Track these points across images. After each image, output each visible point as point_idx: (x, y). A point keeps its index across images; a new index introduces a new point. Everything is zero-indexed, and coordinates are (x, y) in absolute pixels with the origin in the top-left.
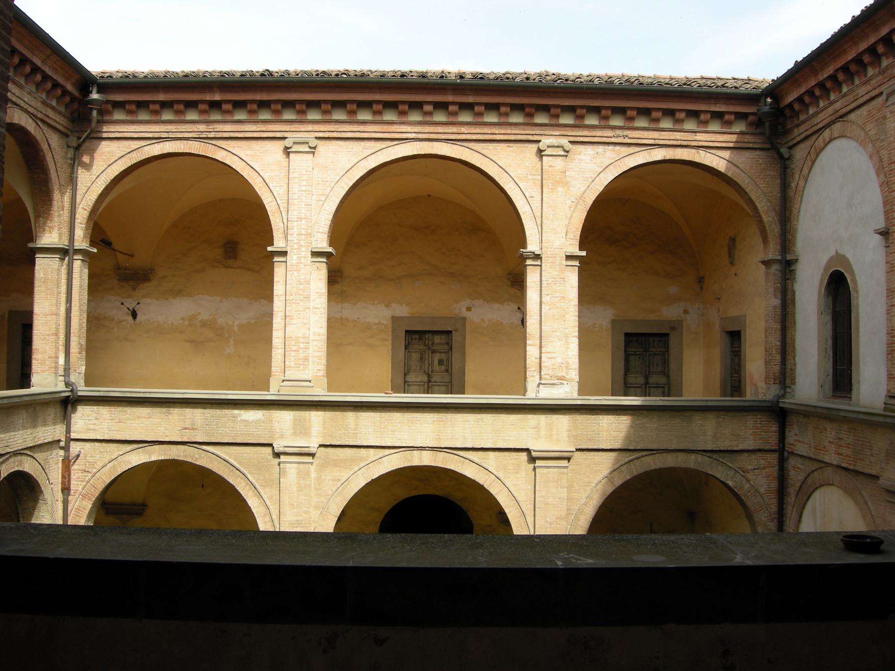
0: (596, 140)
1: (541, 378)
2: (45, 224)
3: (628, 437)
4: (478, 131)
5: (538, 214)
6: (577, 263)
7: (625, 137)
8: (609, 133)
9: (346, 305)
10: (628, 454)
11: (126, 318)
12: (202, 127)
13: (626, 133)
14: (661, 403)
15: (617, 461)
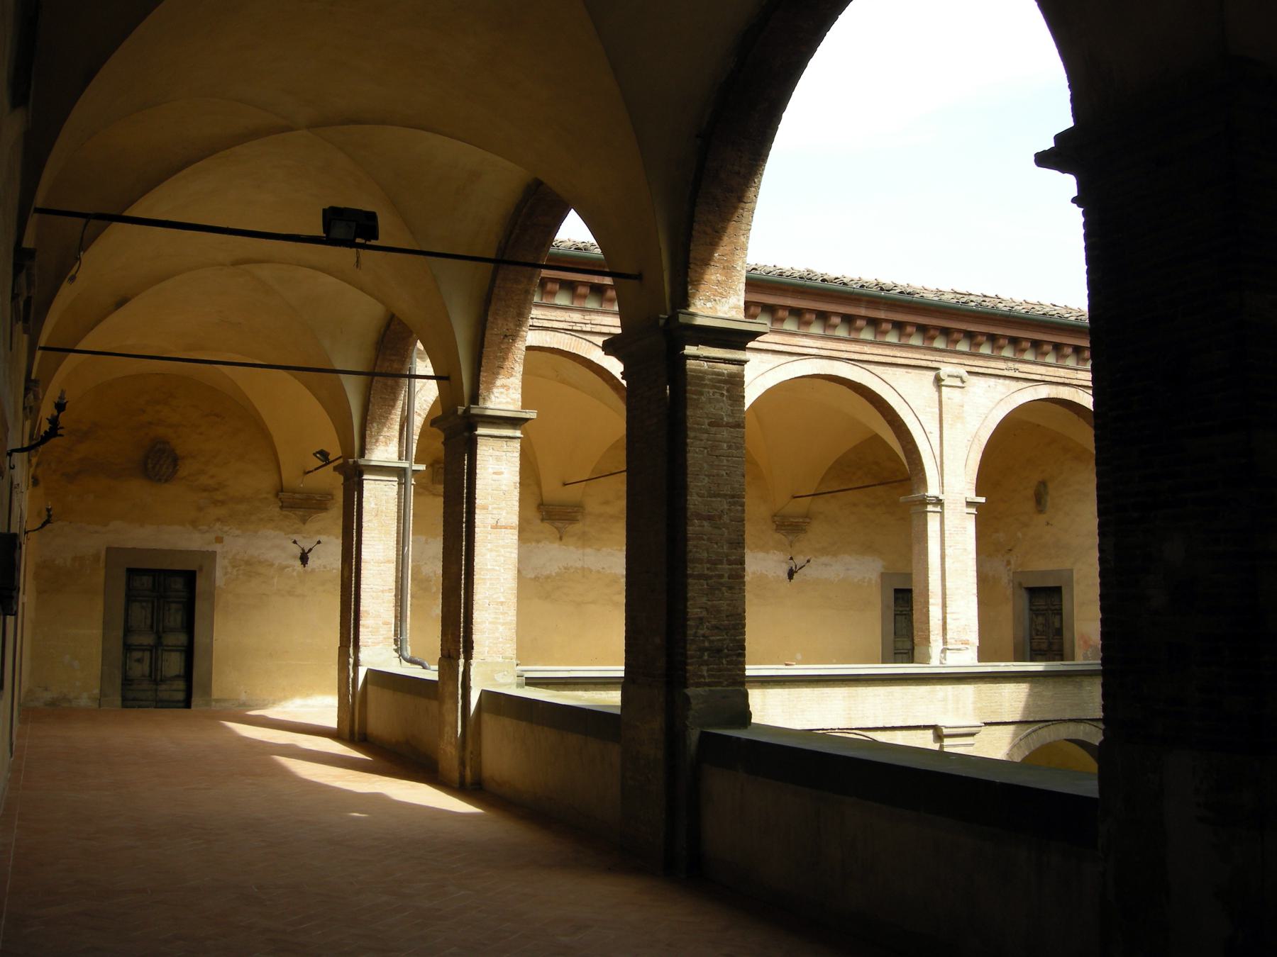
0: (989, 371)
1: (945, 642)
2: (379, 432)
3: (1027, 708)
4: (904, 355)
5: (937, 453)
6: (973, 510)
7: (1016, 370)
8: (1001, 365)
9: (589, 551)
10: (1027, 726)
11: (291, 562)
12: (576, 317)
13: (1018, 366)
14: (1062, 668)
15: (1015, 735)
